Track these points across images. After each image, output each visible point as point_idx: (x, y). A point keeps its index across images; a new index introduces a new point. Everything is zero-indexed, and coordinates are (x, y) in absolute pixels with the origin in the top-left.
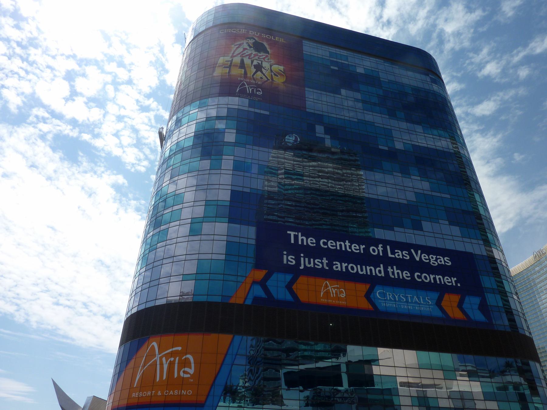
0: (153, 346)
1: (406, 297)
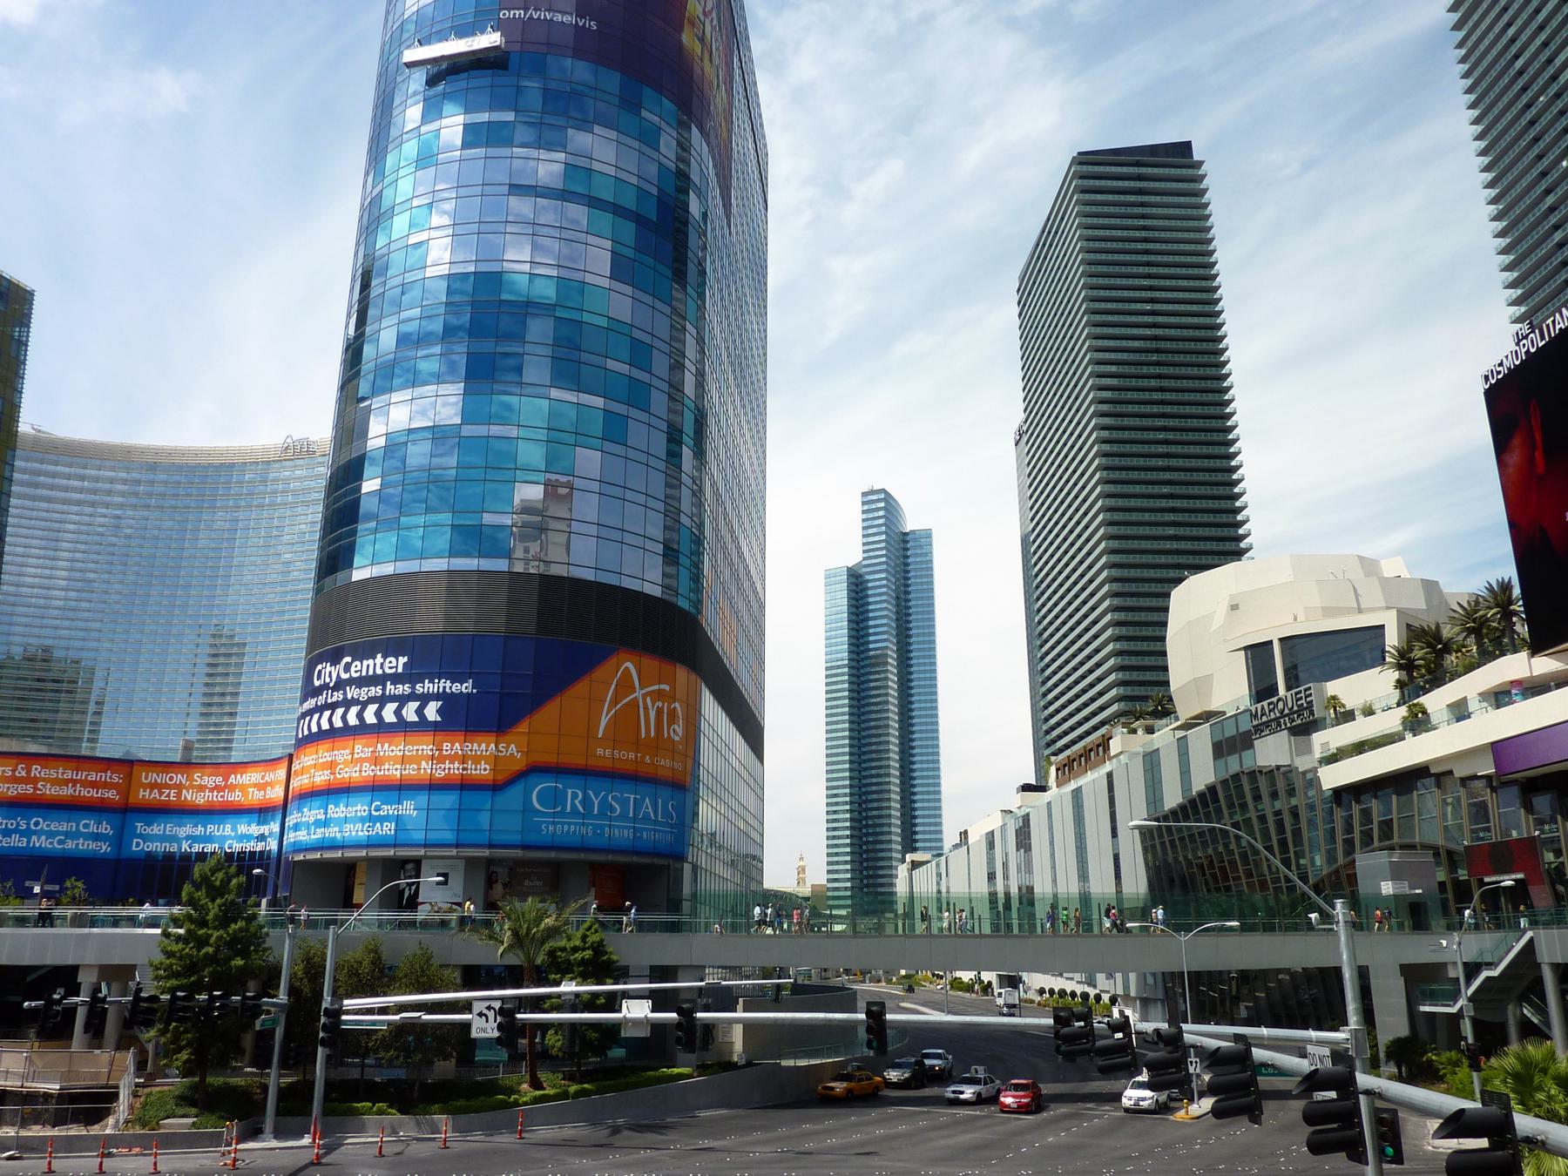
1: (624, 803)
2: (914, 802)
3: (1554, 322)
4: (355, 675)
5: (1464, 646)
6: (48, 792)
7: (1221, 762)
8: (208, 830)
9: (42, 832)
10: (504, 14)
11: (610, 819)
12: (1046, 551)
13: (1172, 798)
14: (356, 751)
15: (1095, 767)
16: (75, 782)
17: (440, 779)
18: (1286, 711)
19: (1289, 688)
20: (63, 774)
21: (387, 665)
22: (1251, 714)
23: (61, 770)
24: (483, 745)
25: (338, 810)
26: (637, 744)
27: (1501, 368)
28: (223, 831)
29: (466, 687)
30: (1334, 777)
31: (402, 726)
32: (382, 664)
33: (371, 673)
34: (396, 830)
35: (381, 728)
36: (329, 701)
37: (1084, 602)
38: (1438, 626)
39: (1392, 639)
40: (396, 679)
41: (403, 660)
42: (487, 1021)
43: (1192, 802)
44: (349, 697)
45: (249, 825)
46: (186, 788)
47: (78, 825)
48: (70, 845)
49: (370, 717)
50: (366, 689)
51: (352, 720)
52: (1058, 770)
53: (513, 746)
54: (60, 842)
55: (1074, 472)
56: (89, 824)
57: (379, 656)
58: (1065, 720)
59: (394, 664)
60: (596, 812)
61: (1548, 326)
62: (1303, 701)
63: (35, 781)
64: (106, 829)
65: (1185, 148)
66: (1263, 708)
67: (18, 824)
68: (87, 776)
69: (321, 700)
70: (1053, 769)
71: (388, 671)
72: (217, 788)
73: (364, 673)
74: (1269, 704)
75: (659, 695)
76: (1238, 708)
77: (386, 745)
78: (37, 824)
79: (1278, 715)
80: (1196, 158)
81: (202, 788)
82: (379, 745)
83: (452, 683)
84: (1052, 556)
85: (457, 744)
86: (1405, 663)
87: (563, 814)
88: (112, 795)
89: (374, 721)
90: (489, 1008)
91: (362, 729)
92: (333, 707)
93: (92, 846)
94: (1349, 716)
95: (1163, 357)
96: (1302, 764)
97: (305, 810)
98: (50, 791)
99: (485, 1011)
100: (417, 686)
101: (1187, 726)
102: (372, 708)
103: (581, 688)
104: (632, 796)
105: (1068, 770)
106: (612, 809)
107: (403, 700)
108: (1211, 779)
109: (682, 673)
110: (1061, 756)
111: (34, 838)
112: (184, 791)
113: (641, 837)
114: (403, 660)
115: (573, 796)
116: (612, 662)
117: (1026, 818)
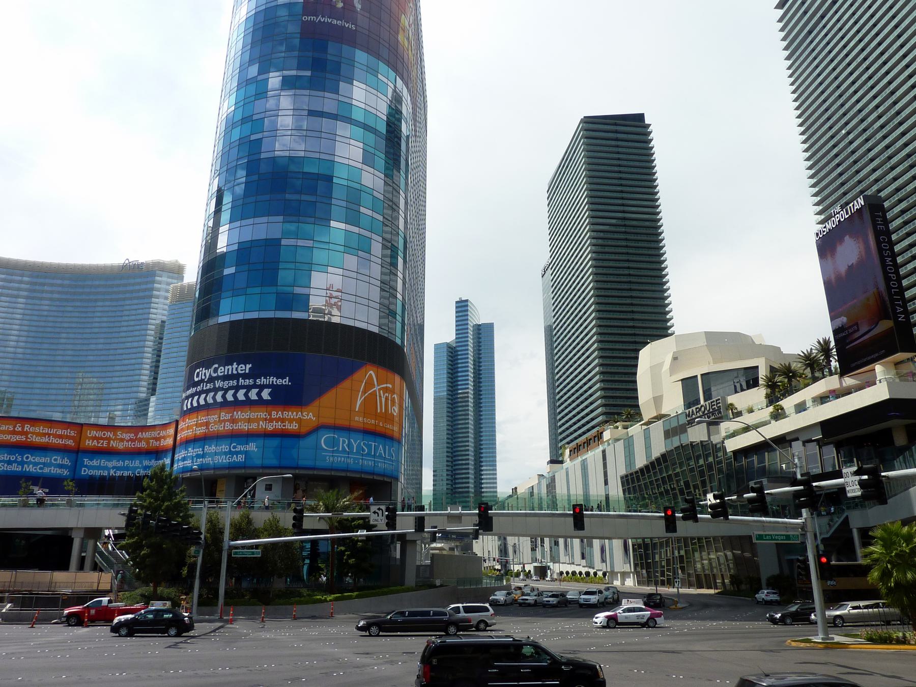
0: (371, 374)
1: (369, 447)
2: (482, 475)
3: (853, 205)
4: (220, 374)
5: (803, 374)
6: (34, 440)
7: (669, 441)
8: (126, 464)
9: (30, 463)
10: (305, 18)
11: (363, 455)
12: (562, 334)
13: (640, 462)
14: (222, 416)
15: (592, 448)
16: (49, 435)
17: (270, 431)
18: (706, 412)
19: (705, 401)
20: (43, 430)
21: (239, 369)
22: (686, 415)
23: (41, 428)
24: (295, 413)
25: (210, 448)
26: (376, 416)
27: (825, 229)
28: (135, 464)
29: (286, 381)
30: (732, 445)
31: (248, 403)
32: (237, 369)
33: (230, 373)
34: (245, 459)
35: (236, 404)
36: (205, 388)
37: (584, 361)
38: (789, 364)
39: (763, 373)
40: (245, 376)
41: (249, 366)
42: (378, 516)
43: (652, 463)
44: (217, 386)
45: (150, 461)
46: (112, 439)
47: (51, 459)
48: (46, 470)
49: (230, 397)
50: (227, 382)
51: (210, 400)
52: (570, 451)
53: (311, 414)
54: (40, 469)
55: (579, 290)
56: (58, 459)
57: (235, 364)
58: (571, 426)
59: (244, 368)
60: (355, 451)
61: (850, 207)
62: (715, 406)
63: (26, 433)
64: (67, 462)
65: (640, 117)
66: (693, 410)
67: (16, 457)
68: (56, 432)
69: (199, 388)
70: (567, 452)
71: (240, 372)
72: (132, 440)
73: (226, 373)
74: (696, 409)
75: (386, 390)
76: (677, 413)
77: (239, 412)
78: (27, 458)
79: (701, 414)
80: (647, 122)
81: (122, 440)
82: (235, 412)
83: (277, 379)
84: (565, 336)
85: (280, 412)
86: (772, 385)
87: (337, 451)
88: (70, 443)
89: (232, 399)
90: (379, 509)
91: (225, 404)
92: (207, 392)
93: (59, 471)
94: (739, 414)
95: (628, 230)
96: (715, 439)
97: (190, 449)
98: (36, 439)
99: (377, 511)
100: (257, 381)
101: (649, 423)
102: (231, 392)
103: (346, 384)
104: (373, 444)
105: (576, 451)
106: (364, 450)
107: (249, 388)
108: (663, 450)
109: (397, 378)
110: (571, 445)
111: (26, 466)
112: (112, 442)
113: (378, 466)
114: (249, 366)
115: (343, 441)
116: (363, 370)
117: (553, 479)
